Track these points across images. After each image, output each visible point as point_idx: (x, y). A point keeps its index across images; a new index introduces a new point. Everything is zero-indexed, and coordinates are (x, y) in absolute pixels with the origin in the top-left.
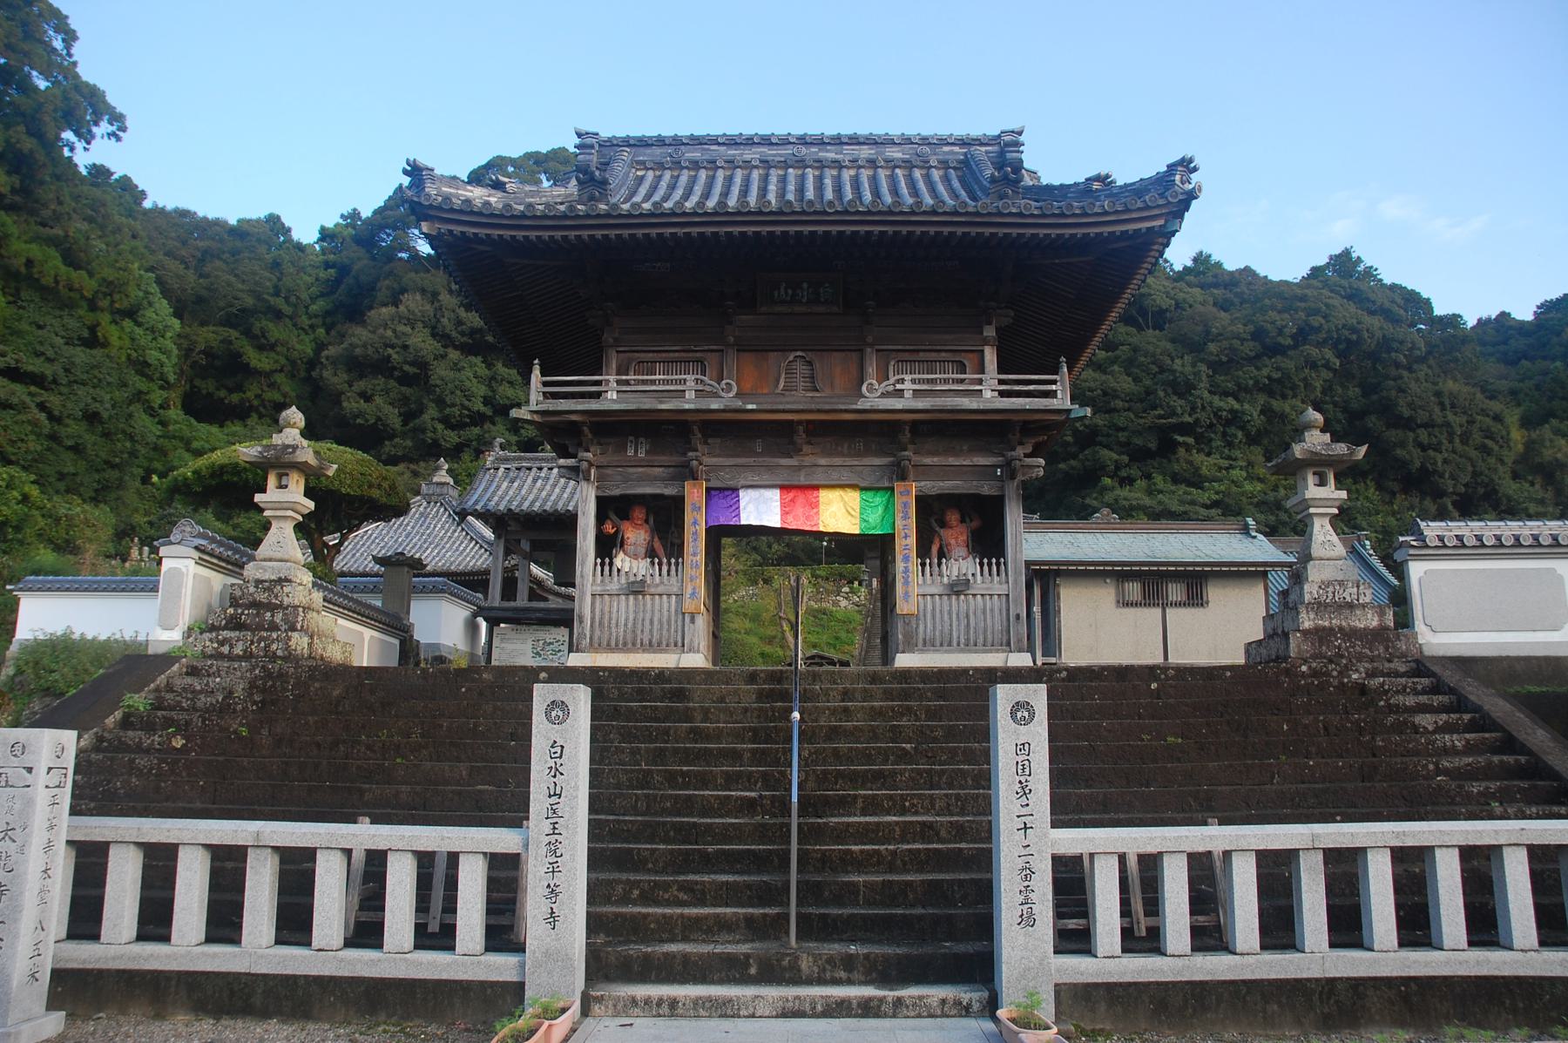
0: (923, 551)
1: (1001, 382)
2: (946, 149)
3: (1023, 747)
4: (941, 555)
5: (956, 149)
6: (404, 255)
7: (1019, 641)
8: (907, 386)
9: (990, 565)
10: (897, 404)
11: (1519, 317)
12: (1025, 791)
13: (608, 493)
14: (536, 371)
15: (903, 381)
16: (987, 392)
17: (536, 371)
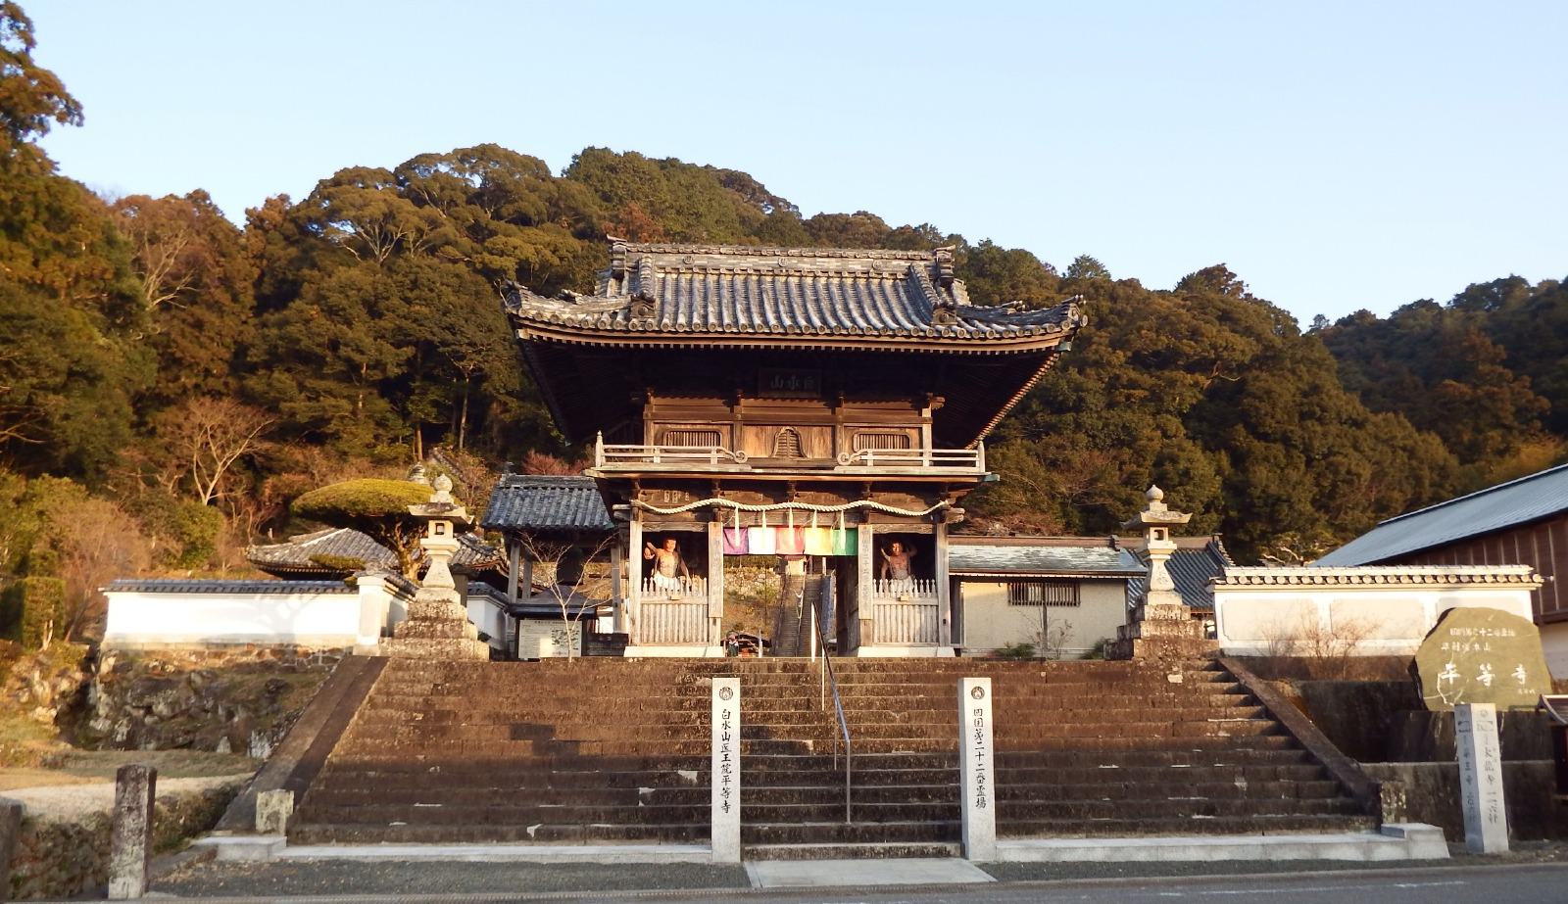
0: (877, 575)
1: (934, 455)
2: (895, 263)
3: (979, 711)
4: (889, 576)
5: (902, 263)
6: (35, 83)
7: (945, 638)
8: (870, 457)
9: (925, 584)
10: (863, 470)
11: (1378, 317)
12: (726, 791)
13: (650, 530)
14: (600, 439)
15: (866, 454)
16: (923, 462)
17: (600, 439)
